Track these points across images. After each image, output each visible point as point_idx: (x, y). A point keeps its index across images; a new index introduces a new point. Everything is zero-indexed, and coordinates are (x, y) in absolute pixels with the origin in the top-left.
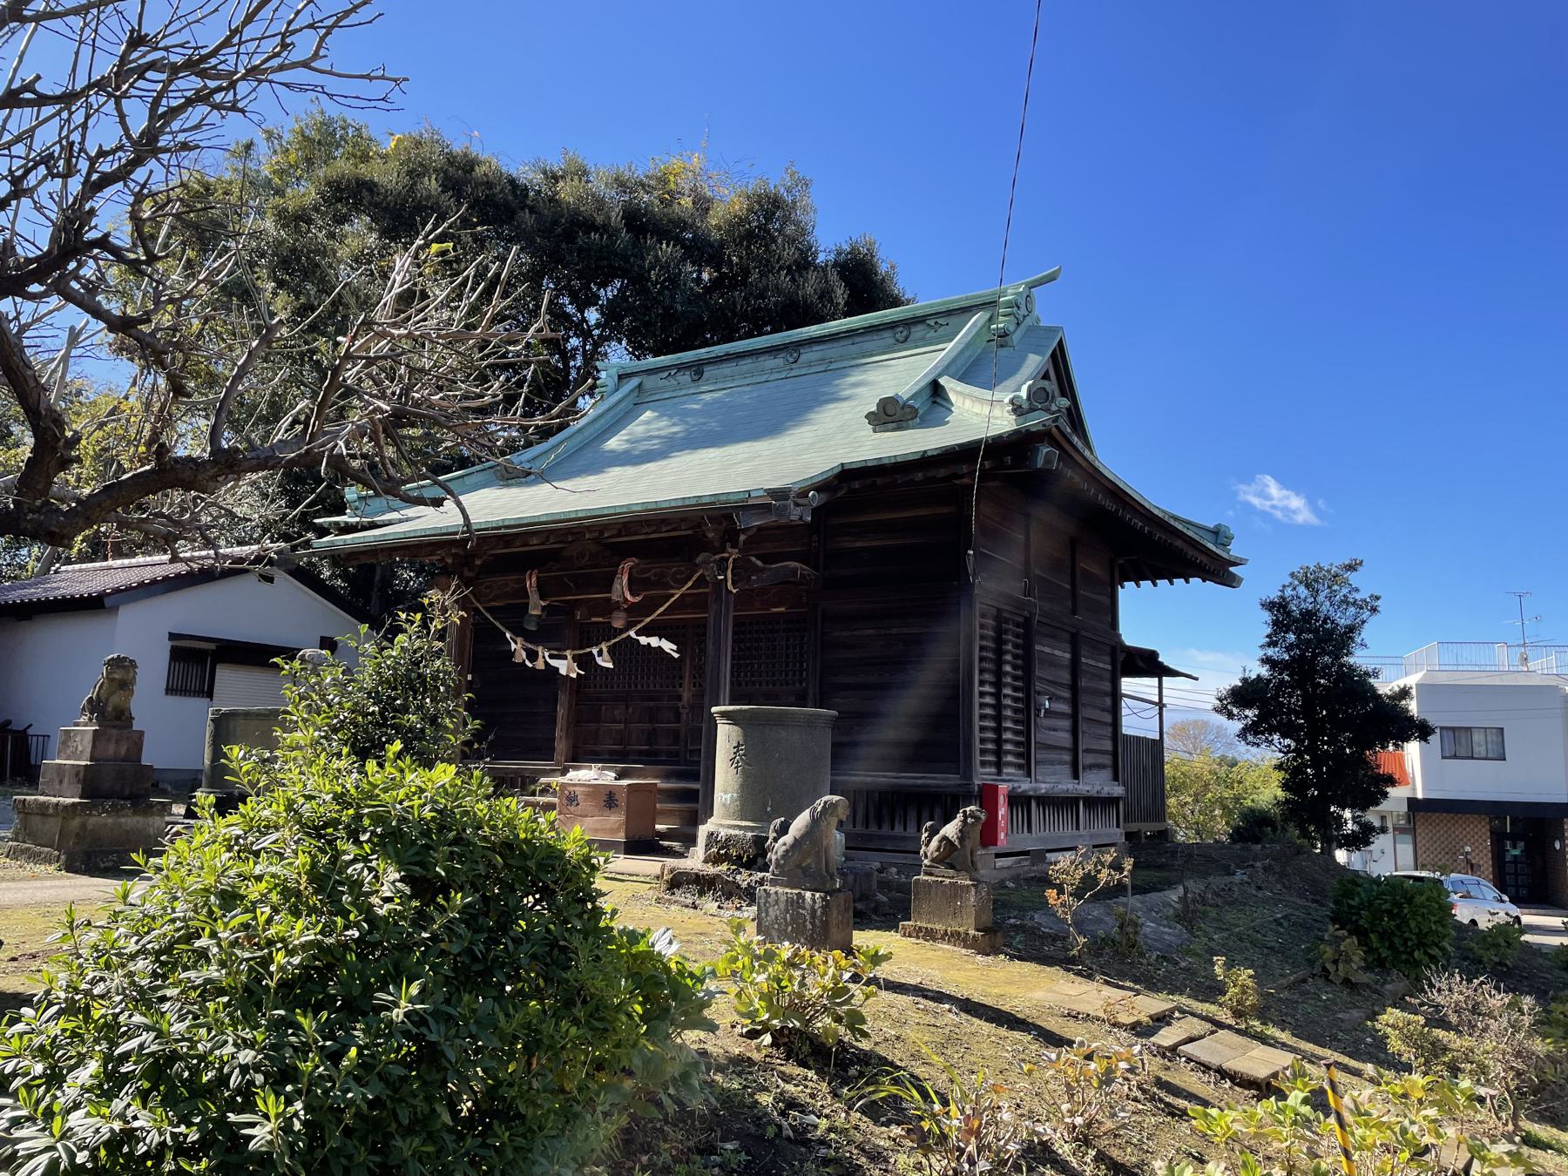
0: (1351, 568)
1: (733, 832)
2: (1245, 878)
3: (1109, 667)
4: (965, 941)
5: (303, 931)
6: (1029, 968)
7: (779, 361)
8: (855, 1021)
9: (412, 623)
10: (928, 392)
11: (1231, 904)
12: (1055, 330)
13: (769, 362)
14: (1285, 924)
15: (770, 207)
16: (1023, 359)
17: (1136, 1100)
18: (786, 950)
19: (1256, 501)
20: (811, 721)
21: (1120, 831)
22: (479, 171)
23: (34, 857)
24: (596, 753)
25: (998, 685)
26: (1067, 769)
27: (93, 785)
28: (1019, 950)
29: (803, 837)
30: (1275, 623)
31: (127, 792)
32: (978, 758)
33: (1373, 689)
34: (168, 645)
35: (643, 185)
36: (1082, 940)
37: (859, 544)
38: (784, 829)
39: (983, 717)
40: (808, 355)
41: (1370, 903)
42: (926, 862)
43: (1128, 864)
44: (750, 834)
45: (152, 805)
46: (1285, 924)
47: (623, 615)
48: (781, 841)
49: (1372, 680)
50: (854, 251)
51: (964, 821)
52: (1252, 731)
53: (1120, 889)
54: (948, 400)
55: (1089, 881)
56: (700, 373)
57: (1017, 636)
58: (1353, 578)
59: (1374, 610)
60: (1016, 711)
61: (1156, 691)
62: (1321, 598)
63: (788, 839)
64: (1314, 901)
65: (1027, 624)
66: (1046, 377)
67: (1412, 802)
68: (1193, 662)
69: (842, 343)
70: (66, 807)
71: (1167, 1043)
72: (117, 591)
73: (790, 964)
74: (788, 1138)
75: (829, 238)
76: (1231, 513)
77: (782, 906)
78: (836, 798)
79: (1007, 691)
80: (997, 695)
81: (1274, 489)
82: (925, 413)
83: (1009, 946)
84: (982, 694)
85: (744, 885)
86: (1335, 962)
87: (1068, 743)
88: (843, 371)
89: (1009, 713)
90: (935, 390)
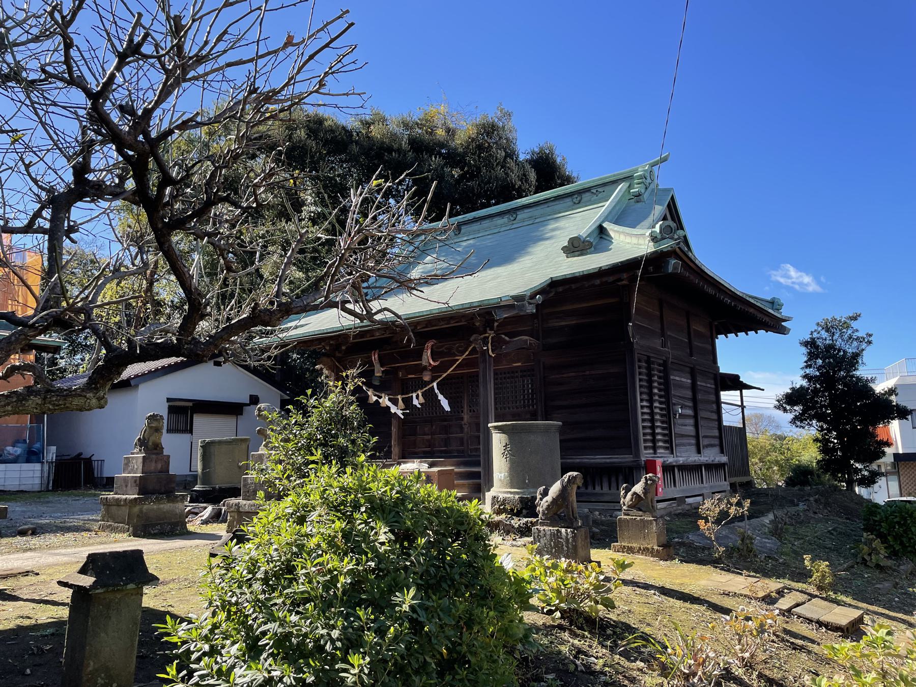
0: (854, 318)
1: (509, 495)
2: (805, 507)
3: (713, 386)
4: (652, 553)
5: (348, 564)
6: (692, 567)
7: (505, 220)
8: (609, 605)
9: (337, 387)
10: (597, 232)
11: (801, 523)
12: (669, 190)
13: (499, 221)
14: (835, 533)
15: (490, 129)
16: (651, 208)
17: (773, 641)
18: (563, 563)
19: (782, 280)
20: (547, 429)
21: (727, 483)
22: (326, 124)
23: (114, 530)
24: (416, 453)
25: (651, 401)
26: (694, 448)
27: (146, 487)
28: (684, 557)
29: (557, 497)
30: (809, 354)
31: (163, 490)
32: (642, 445)
33: (872, 390)
34: (166, 405)
35: (417, 124)
36: (722, 549)
37: (563, 323)
38: (545, 493)
39: (644, 420)
40: (521, 215)
41: (887, 518)
42: (625, 508)
43: (747, 504)
44: (517, 497)
45: (177, 497)
46: (835, 533)
47: (429, 373)
48: (545, 499)
49: (871, 385)
50: (541, 150)
51: (646, 483)
52: (798, 420)
53: (741, 518)
54: (609, 236)
55: (724, 514)
57: (660, 371)
58: (854, 324)
59: (870, 342)
60: (662, 415)
61: (739, 398)
63: (549, 498)
64: (847, 519)
65: (665, 364)
66: (665, 219)
67: (896, 456)
68: (762, 379)
69: (542, 206)
70: (131, 501)
71: (785, 607)
72: (137, 376)
73: (567, 571)
74: (582, 671)
75: (525, 147)
76: (767, 288)
77: (548, 537)
78: (575, 473)
79: (656, 404)
80: (651, 407)
81: (793, 273)
82: (597, 244)
83: (677, 554)
84: (642, 407)
85: (517, 526)
86: (870, 555)
87: (693, 433)
88: (544, 223)
89: (658, 417)
90: (601, 231)
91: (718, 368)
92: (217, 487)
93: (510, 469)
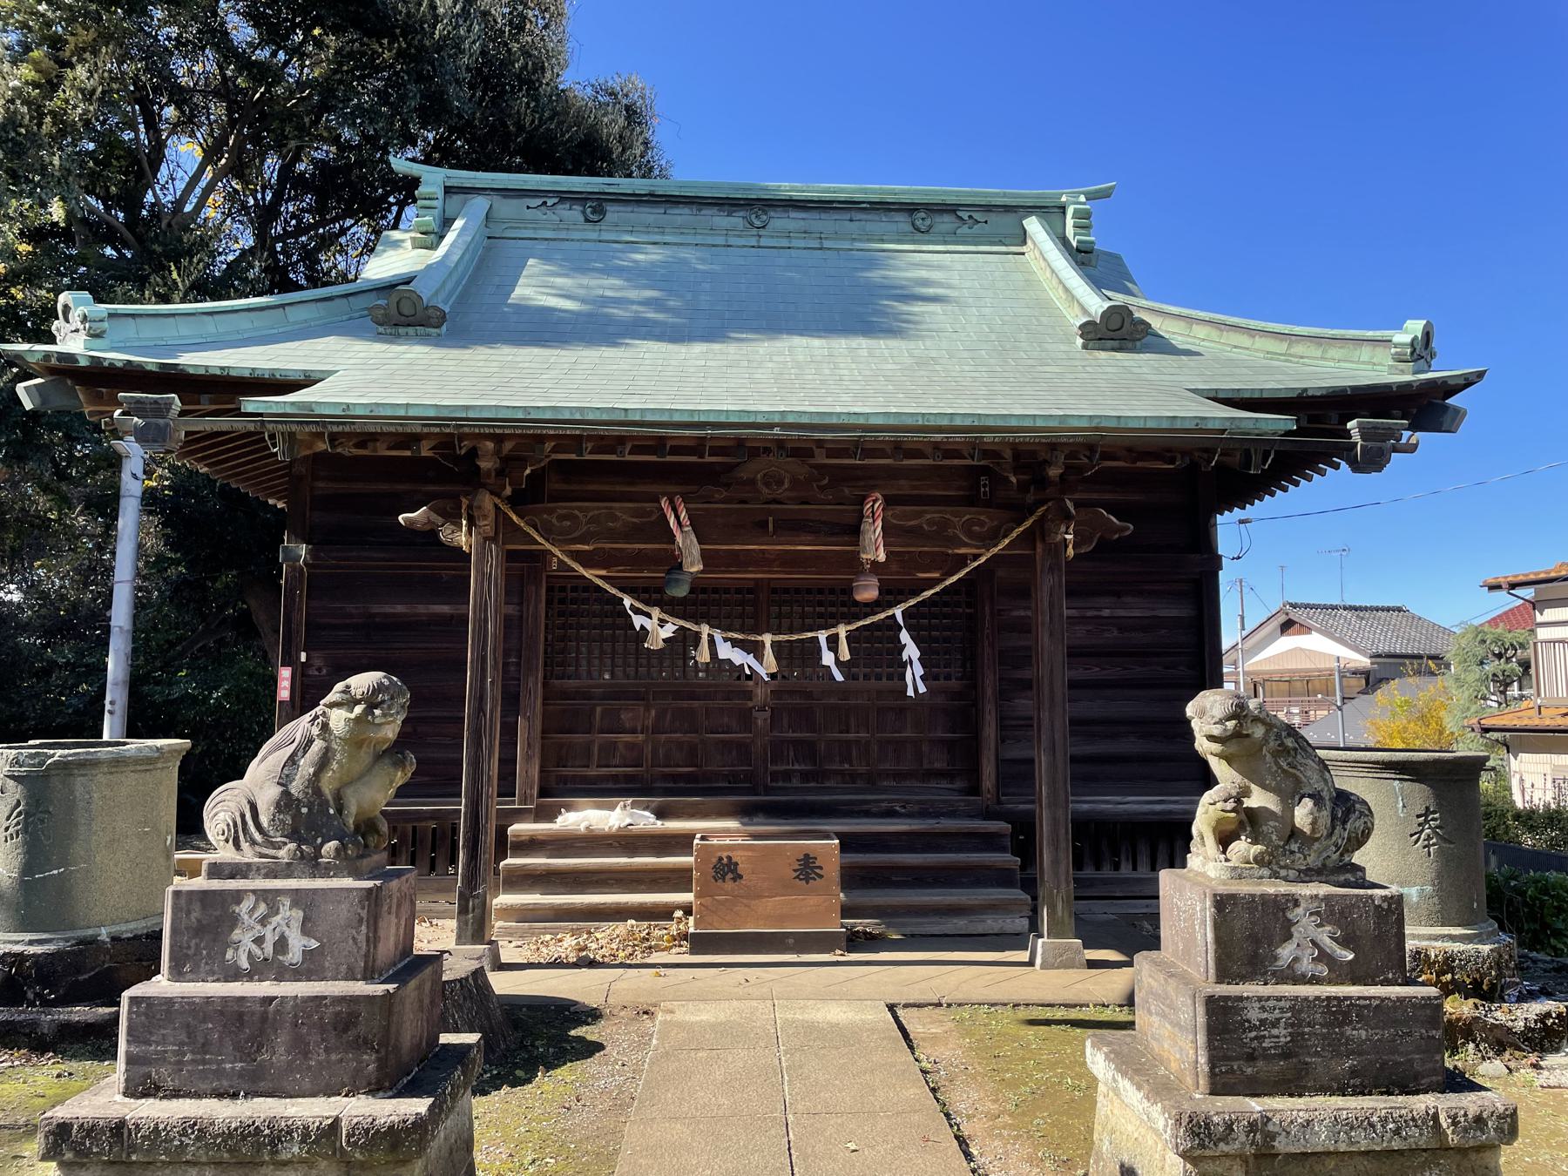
7: (737, 220)
56: (600, 211)
92: (104, 934)
93: (1439, 875)
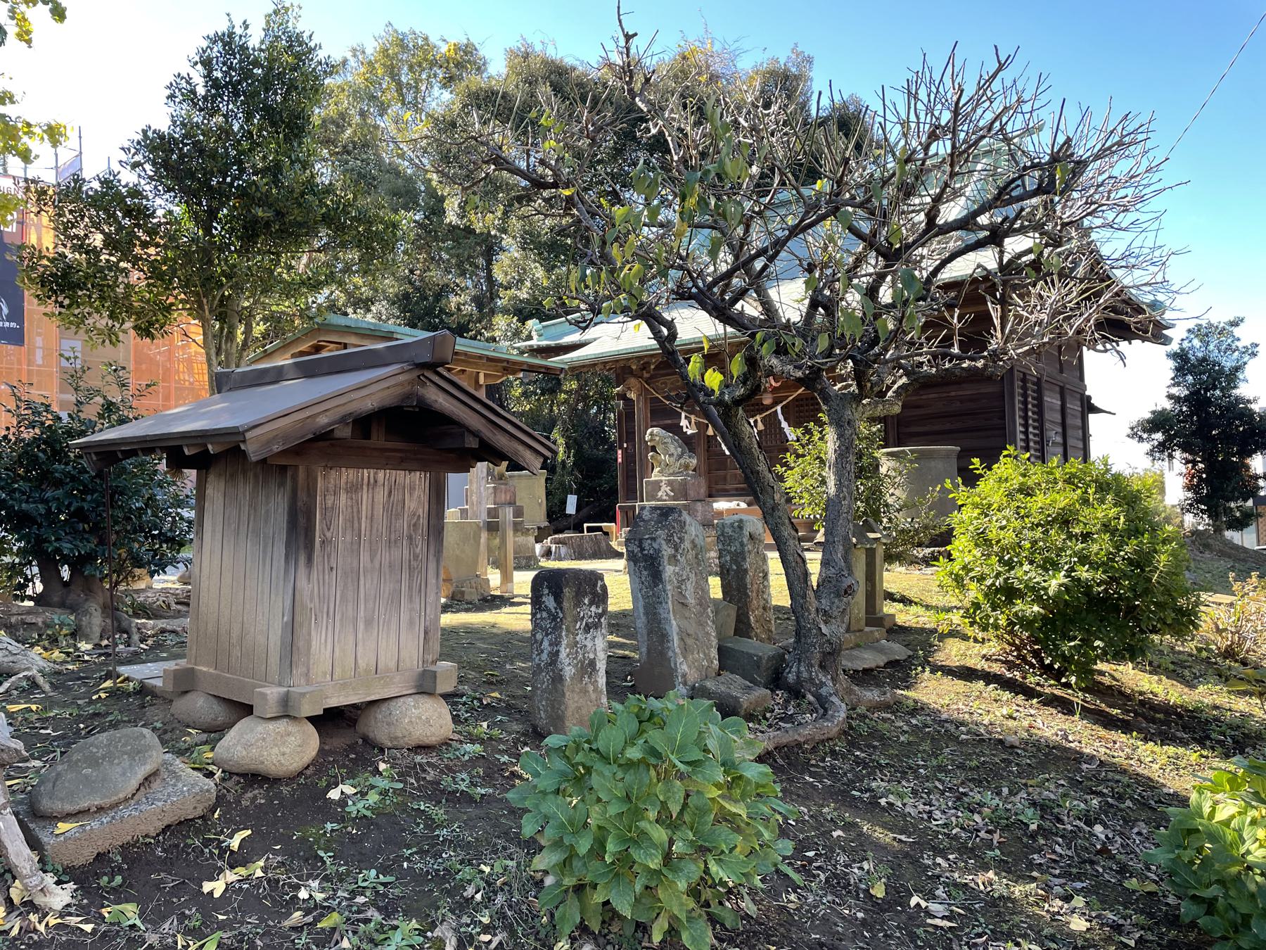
0: (1235, 324)
20: (948, 455)
30: (1177, 369)
47: (770, 395)
58: (1237, 331)
62: (1211, 347)
91: (1085, 388)
